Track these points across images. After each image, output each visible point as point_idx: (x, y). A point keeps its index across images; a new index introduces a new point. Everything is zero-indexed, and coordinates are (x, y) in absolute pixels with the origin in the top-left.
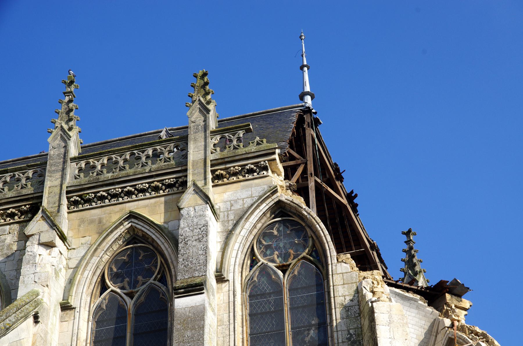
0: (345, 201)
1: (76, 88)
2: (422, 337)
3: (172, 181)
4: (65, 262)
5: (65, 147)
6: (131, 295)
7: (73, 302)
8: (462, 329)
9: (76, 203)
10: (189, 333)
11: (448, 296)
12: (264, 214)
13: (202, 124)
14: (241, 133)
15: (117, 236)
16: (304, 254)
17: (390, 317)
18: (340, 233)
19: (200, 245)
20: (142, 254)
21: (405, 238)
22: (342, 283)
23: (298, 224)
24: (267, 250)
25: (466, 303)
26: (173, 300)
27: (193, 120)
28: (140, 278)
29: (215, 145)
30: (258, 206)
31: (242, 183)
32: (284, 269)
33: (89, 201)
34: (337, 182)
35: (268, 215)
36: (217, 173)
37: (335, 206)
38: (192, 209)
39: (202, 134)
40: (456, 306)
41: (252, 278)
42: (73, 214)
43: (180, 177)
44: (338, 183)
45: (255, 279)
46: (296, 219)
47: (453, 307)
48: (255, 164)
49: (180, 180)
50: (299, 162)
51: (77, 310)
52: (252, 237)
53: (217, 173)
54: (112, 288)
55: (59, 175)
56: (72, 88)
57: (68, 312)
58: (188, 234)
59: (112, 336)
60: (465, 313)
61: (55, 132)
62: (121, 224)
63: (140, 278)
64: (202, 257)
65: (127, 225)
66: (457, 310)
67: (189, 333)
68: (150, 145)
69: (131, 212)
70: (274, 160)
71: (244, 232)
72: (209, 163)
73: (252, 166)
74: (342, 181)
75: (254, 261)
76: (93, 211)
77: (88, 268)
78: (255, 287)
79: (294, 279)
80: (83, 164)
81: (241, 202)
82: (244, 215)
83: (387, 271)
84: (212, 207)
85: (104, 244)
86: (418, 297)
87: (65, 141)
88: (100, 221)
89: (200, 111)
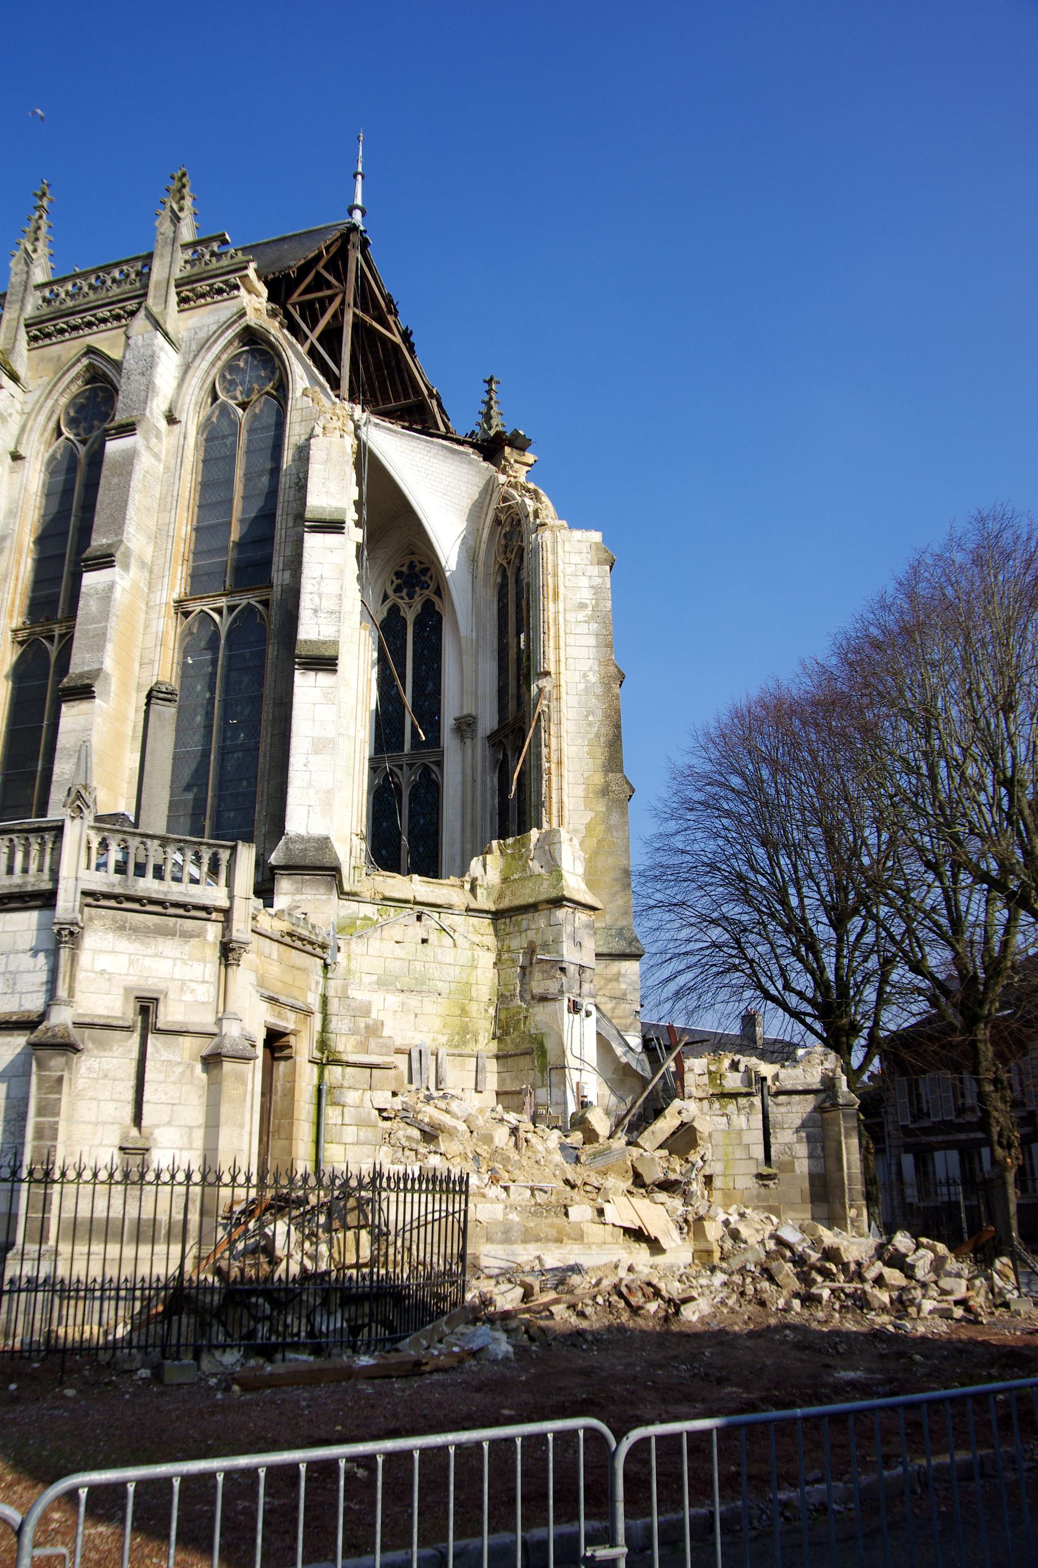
0: (398, 339)
1: (51, 201)
2: (476, 497)
4: (19, 407)
5: (28, 273)
6: (83, 442)
7: (22, 451)
8: (515, 486)
9: (35, 339)
10: (116, 480)
11: (507, 449)
12: (230, 343)
13: (172, 235)
14: (215, 247)
15: (73, 375)
16: (268, 388)
17: (329, 454)
18: (397, 378)
19: (144, 380)
20: (101, 395)
21: (486, 387)
22: (299, 419)
23: (267, 353)
24: (230, 386)
25: (530, 458)
27: (162, 231)
28: (96, 423)
29: (186, 262)
30: (223, 333)
31: (210, 307)
32: (243, 406)
33: (48, 335)
34: (389, 317)
35: (236, 344)
37: (389, 346)
38: (140, 337)
39: (169, 249)
40: (516, 461)
41: (209, 419)
42: (34, 352)
44: (391, 319)
45: (214, 420)
46: (265, 347)
47: (512, 461)
48: (225, 282)
50: (338, 290)
51: (28, 459)
52: (215, 371)
53: (183, 295)
55: (17, 306)
56: (45, 203)
57: (19, 462)
58: (132, 367)
59: (60, 489)
60: (529, 468)
61: (17, 254)
62: (79, 360)
64: (143, 393)
65: (85, 361)
66: (517, 466)
67: (116, 480)
68: (117, 265)
69: (89, 346)
70: (247, 276)
71: (205, 365)
72: (173, 283)
73: (221, 285)
74: (396, 316)
75: (215, 398)
76: (53, 348)
77: (42, 413)
78: (213, 429)
79: (255, 417)
80: (47, 293)
81: (206, 329)
82: (204, 345)
83: (450, 424)
84: (166, 335)
85: (60, 384)
86: (471, 450)
87: (27, 265)
88: (59, 358)
89: (172, 220)
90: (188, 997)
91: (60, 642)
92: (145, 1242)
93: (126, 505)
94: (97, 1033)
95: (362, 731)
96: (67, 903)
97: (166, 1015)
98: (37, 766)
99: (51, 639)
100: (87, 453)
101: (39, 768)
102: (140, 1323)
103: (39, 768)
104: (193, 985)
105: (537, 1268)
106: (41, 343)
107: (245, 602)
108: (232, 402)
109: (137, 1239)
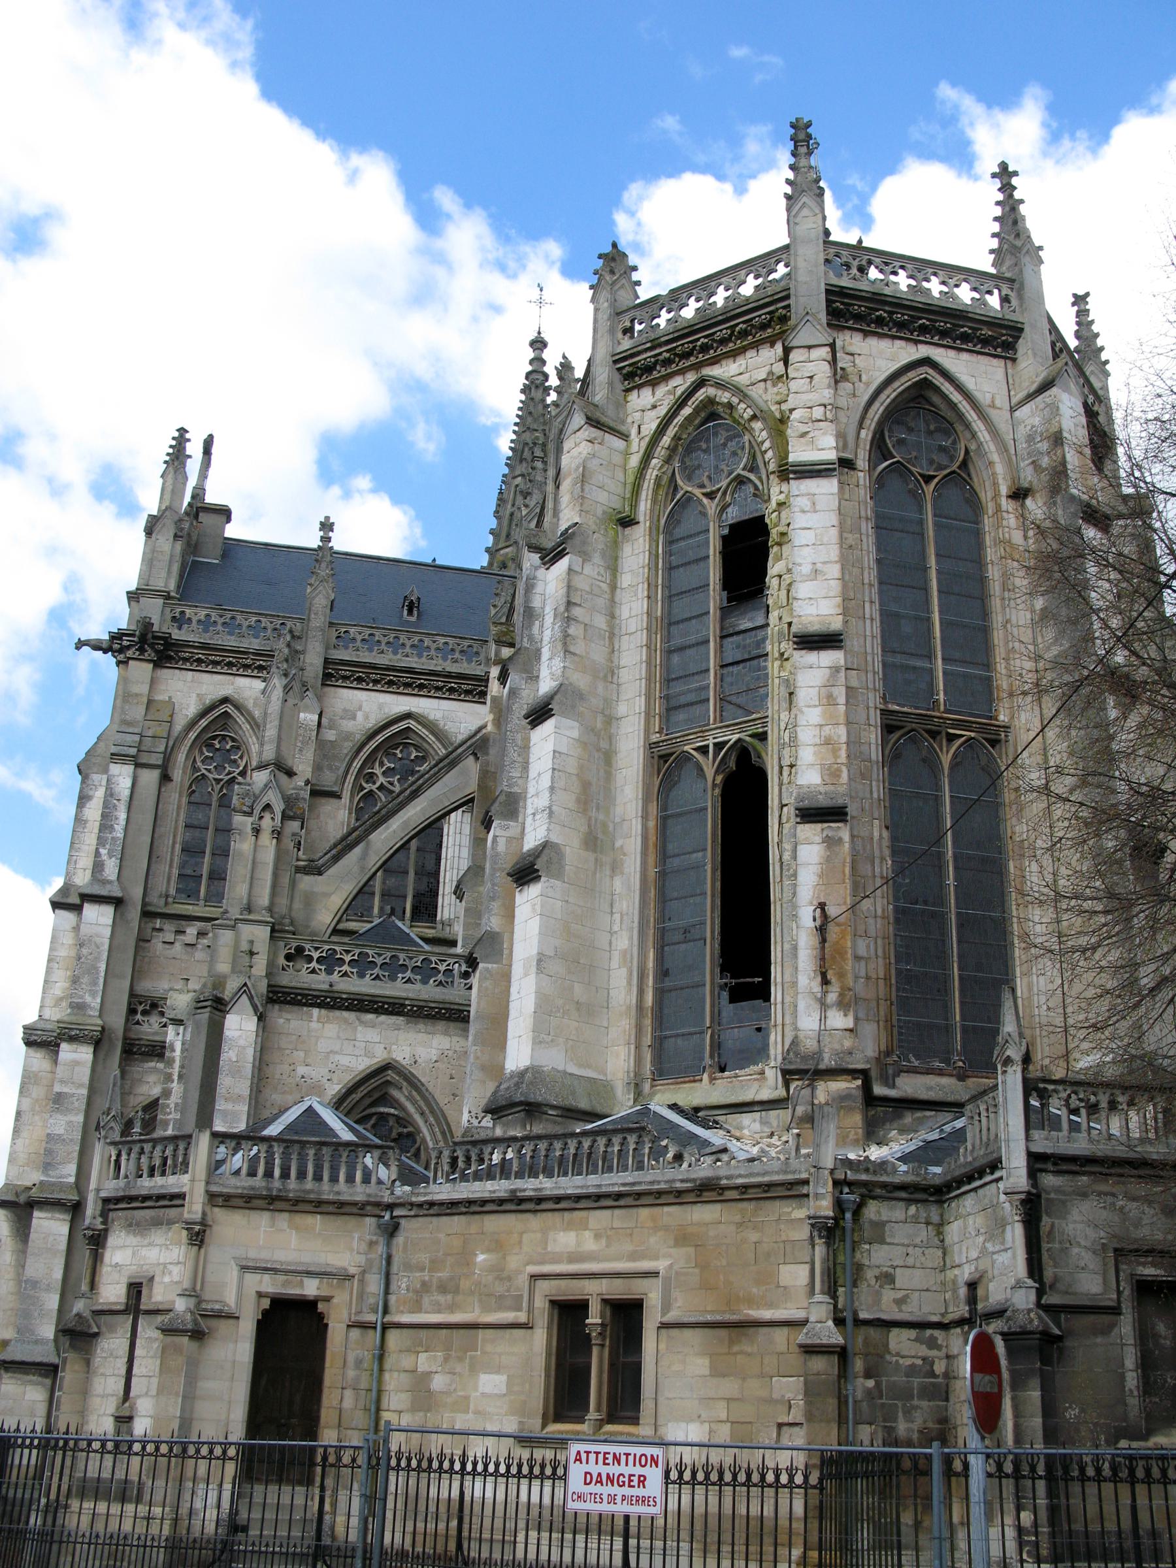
90: (167, 1279)
92: (130, 1501)
94: (108, 1318)
95: (625, 935)
96: (91, 1209)
97: (150, 1297)
104: (170, 1267)
107: (735, 737)
108: (697, 492)
109: (123, 1499)
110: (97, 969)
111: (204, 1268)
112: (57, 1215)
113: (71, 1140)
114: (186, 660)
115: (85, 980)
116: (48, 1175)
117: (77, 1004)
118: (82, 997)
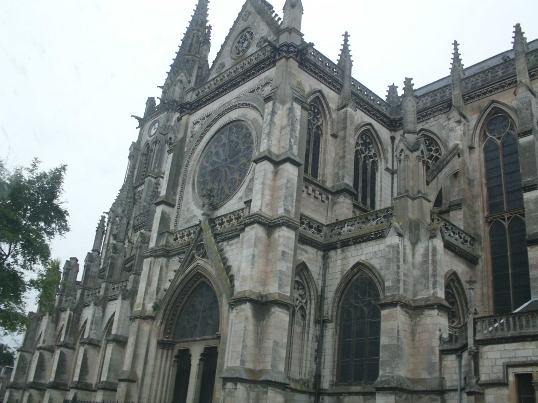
3: (510, 82)
10: (527, 154)
26: (472, 72)
28: (502, 130)
36: (532, 74)
43: (514, 79)
49: (514, 80)
54: (490, 136)
58: (521, 107)
63: (502, 130)
91: (508, 221)
93: (536, 164)
98: (509, 271)
99: (504, 219)
100: (501, 143)
101: (510, 272)
102: (141, 238)
103: (510, 272)
105: (131, 177)
106: (470, 101)
110: (293, 195)
111: (392, 183)
112: (285, 311)
113: (288, 275)
114: (307, 67)
115: (289, 199)
116: (280, 290)
117: (287, 209)
118: (288, 207)
